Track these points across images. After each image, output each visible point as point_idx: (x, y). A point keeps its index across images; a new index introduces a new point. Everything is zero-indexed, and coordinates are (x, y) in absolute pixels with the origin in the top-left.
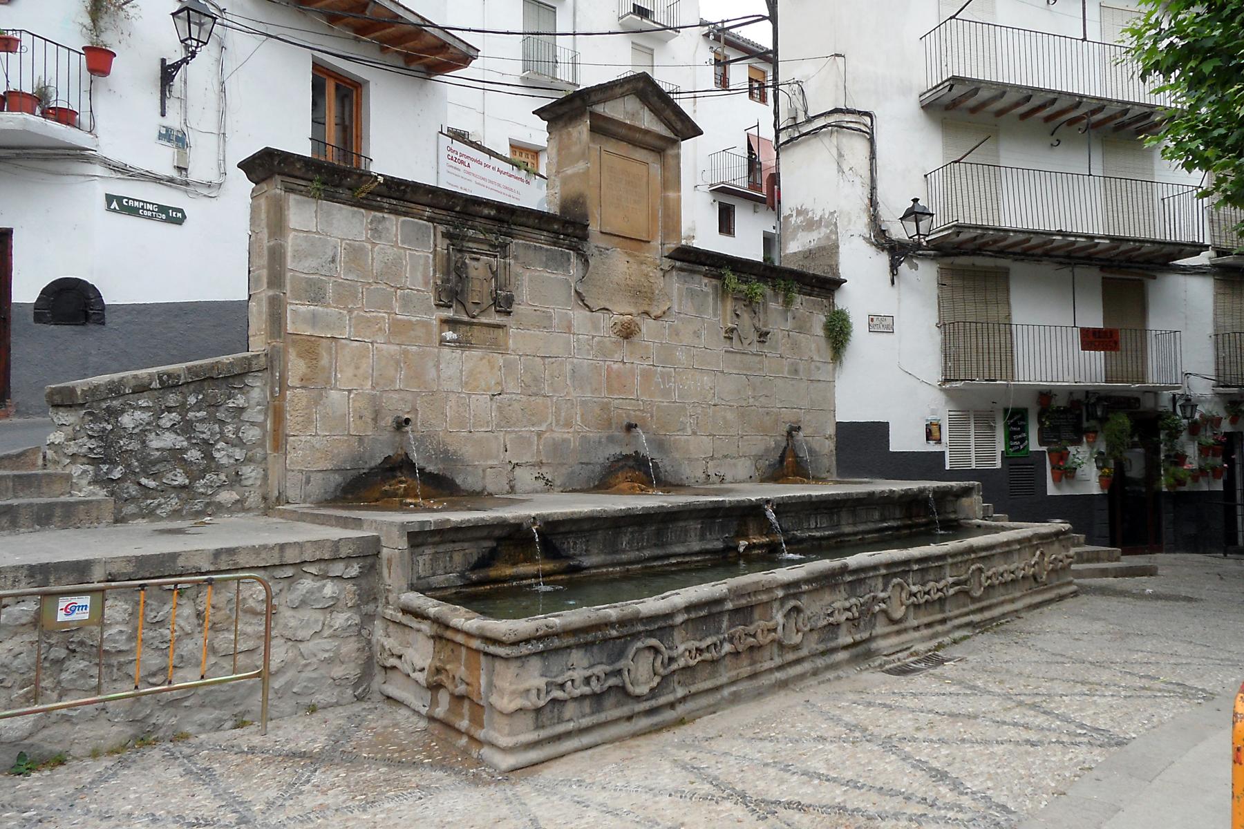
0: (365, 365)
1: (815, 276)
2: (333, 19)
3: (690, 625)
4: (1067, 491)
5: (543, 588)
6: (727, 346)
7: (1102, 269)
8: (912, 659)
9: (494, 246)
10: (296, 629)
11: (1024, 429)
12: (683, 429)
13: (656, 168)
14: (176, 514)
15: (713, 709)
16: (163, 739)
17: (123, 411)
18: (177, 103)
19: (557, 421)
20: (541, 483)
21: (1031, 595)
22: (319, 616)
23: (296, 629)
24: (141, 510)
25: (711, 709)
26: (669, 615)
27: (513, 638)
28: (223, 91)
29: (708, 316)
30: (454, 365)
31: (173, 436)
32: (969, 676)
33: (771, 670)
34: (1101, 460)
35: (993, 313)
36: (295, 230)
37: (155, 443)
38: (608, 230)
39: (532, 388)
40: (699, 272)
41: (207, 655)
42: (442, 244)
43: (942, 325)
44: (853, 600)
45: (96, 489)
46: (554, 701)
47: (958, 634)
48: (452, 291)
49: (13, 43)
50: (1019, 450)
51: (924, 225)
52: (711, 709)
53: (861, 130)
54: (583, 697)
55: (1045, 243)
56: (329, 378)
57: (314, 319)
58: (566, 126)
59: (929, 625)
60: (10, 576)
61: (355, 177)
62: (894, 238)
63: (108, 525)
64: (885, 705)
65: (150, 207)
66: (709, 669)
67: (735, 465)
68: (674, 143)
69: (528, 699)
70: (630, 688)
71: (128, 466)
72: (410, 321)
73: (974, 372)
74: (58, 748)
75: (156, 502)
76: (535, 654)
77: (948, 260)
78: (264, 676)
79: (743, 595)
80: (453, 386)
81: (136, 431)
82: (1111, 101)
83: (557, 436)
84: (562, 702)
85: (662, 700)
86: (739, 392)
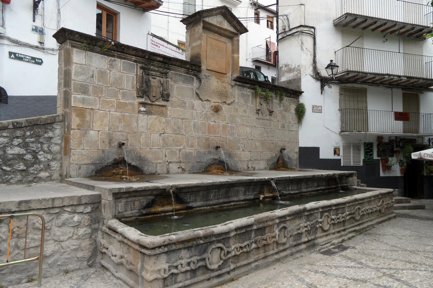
0: (106, 121)
1: (292, 90)
3: (237, 237)
4: (387, 175)
6: (257, 116)
7: (403, 89)
8: (332, 247)
9: (162, 73)
10: (60, 236)
11: (372, 151)
12: (239, 149)
13: (229, 45)
14: (20, 182)
18: (40, 17)
19: (187, 145)
20: (180, 170)
21: (378, 218)
23: (60, 236)
24: (3, 180)
25: (246, 273)
26: (228, 233)
27: (152, 246)
29: (250, 104)
30: (144, 121)
31: (19, 149)
32: (358, 256)
33: (273, 255)
34: (401, 163)
35: (360, 106)
36: (76, 63)
37: (10, 151)
38: (210, 68)
39: (177, 131)
42: (140, 72)
43: (340, 110)
44: (308, 223)
46: (172, 274)
47: (350, 235)
48: (144, 90)
50: (369, 159)
51: (335, 71)
52: (246, 273)
54: (186, 271)
55: (381, 79)
56: (90, 125)
57: (83, 101)
58: (193, 26)
59: (339, 232)
61: (102, 42)
62: (322, 76)
64: (324, 273)
65: (28, 57)
67: (259, 163)
68: (237, 35)
70: (209, 266)
72: (126, 103)
73: (353, 129)
75: (10, 177)
76: (163, 253)
77: (343, 85)
78: (42, 258)
79: (261, 223)
80: (144, 130)
82: (408, 24)
83: (187, 151)
84: (177, 274)
85: (224, 271)
86: (261, 134)
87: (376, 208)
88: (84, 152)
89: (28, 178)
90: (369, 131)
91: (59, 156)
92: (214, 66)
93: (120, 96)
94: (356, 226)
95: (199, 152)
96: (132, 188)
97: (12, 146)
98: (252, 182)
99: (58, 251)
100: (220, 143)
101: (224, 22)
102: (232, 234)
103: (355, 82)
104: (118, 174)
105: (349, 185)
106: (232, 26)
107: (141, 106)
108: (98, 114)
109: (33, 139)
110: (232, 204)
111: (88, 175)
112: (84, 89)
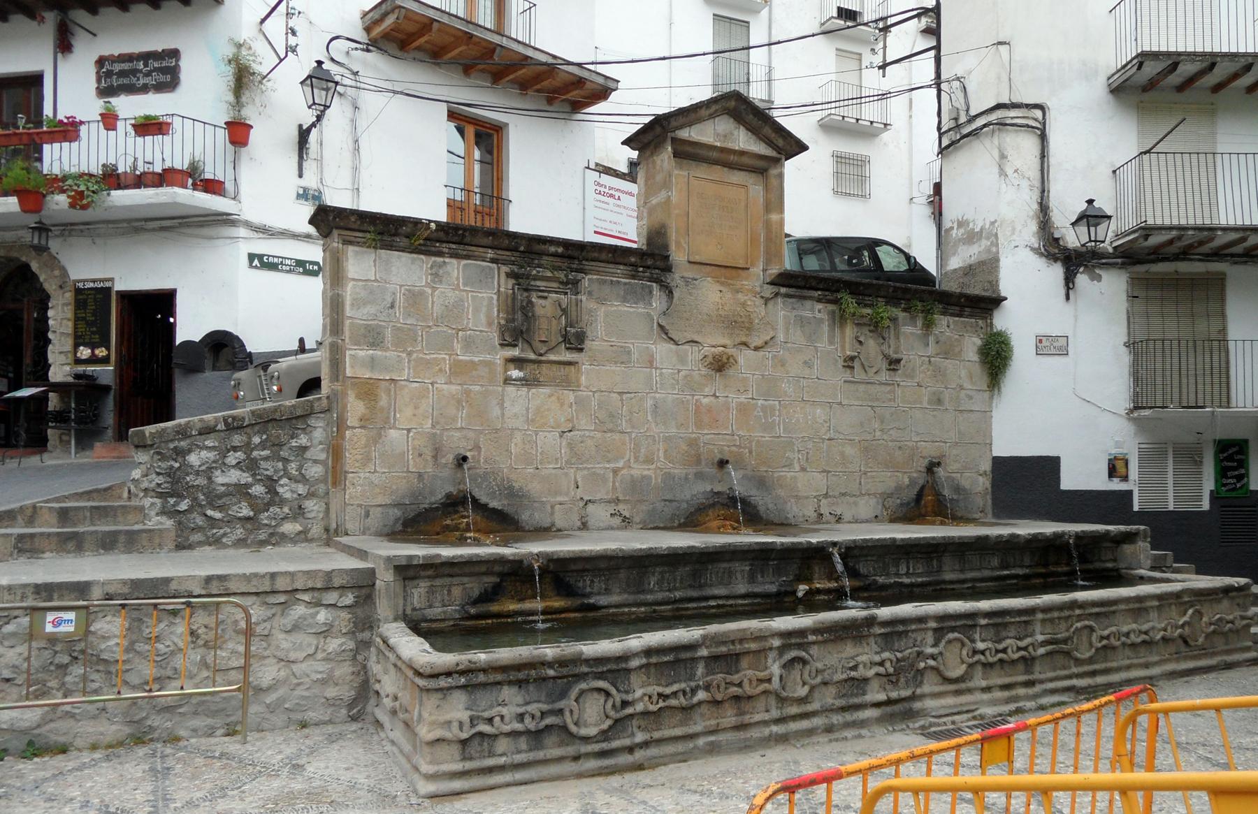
0: (425, 405)
2: (467, 70)
5: (540, 626)
6: (847, 375)
10: (288, 651)
12: (790, 465)
14: (240, 543)
15: (683, 758)
16: (158, 740)
17: (190, 451)
18: (314, 164)
19: (636, 458)
20: (617, 521)
22: (313, 641)
24: (208, 538)
26: (624, 658)
27: (428, 671)
28: (357, 149)
29: (823, 344)
30: (518, 403)
31: (238, 473)
33: (765, 723)
35: (1202, 327)
36: (354, 280)
37: (220, 478)
38: (697, 258)
40: (810, 298)
41: (200, 669)
42: (507, 285)
43: (1131, 345)
44: (886, 655)
45: (163, 519)
48: (518, 327)
49: (164, 127)
50: (1234, 489)
53: (1028, 126)
56: (388, 418)
57: (372, 363)
60: (19, 592)
63: (170, 551)
65: (288, 262)
66: (679, 716)
67: (856, 504)
68: (777, 162)
69: (450, 731)
71: (195, 499)
72: (472, 362)
74: (62, 739)
75: (222, 531)
76: (457, 687)
77: (1141, 269)
79: (724, 643)
80: (519, 423)
81: (203, 468)
84: (494, 737)
86: (862, 424)
87: (1165, 630)
88: (375, 478)
89: (258, 534)
90: (1233, 403)
91: (321, 488)
92: (710, 252)
93: (458, 347)
94: (1078, 676)
95: (668, 477)
96: (439, 556)
97: (224, 467)
98: (772, 550)
99: (285, 681)
100: (731, 452)
101: (736, 133)
102: (635, 663)
103: (1184, 255)
104: (456, 528)
105: (1122, 565)
106: (761, 139)
107: (511, 366)
108: (406, 390)
109: (266, 453)
110: (713, 603)
111: (386, 530)
112: (373, 337)
